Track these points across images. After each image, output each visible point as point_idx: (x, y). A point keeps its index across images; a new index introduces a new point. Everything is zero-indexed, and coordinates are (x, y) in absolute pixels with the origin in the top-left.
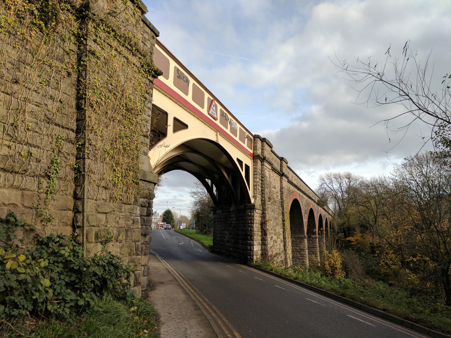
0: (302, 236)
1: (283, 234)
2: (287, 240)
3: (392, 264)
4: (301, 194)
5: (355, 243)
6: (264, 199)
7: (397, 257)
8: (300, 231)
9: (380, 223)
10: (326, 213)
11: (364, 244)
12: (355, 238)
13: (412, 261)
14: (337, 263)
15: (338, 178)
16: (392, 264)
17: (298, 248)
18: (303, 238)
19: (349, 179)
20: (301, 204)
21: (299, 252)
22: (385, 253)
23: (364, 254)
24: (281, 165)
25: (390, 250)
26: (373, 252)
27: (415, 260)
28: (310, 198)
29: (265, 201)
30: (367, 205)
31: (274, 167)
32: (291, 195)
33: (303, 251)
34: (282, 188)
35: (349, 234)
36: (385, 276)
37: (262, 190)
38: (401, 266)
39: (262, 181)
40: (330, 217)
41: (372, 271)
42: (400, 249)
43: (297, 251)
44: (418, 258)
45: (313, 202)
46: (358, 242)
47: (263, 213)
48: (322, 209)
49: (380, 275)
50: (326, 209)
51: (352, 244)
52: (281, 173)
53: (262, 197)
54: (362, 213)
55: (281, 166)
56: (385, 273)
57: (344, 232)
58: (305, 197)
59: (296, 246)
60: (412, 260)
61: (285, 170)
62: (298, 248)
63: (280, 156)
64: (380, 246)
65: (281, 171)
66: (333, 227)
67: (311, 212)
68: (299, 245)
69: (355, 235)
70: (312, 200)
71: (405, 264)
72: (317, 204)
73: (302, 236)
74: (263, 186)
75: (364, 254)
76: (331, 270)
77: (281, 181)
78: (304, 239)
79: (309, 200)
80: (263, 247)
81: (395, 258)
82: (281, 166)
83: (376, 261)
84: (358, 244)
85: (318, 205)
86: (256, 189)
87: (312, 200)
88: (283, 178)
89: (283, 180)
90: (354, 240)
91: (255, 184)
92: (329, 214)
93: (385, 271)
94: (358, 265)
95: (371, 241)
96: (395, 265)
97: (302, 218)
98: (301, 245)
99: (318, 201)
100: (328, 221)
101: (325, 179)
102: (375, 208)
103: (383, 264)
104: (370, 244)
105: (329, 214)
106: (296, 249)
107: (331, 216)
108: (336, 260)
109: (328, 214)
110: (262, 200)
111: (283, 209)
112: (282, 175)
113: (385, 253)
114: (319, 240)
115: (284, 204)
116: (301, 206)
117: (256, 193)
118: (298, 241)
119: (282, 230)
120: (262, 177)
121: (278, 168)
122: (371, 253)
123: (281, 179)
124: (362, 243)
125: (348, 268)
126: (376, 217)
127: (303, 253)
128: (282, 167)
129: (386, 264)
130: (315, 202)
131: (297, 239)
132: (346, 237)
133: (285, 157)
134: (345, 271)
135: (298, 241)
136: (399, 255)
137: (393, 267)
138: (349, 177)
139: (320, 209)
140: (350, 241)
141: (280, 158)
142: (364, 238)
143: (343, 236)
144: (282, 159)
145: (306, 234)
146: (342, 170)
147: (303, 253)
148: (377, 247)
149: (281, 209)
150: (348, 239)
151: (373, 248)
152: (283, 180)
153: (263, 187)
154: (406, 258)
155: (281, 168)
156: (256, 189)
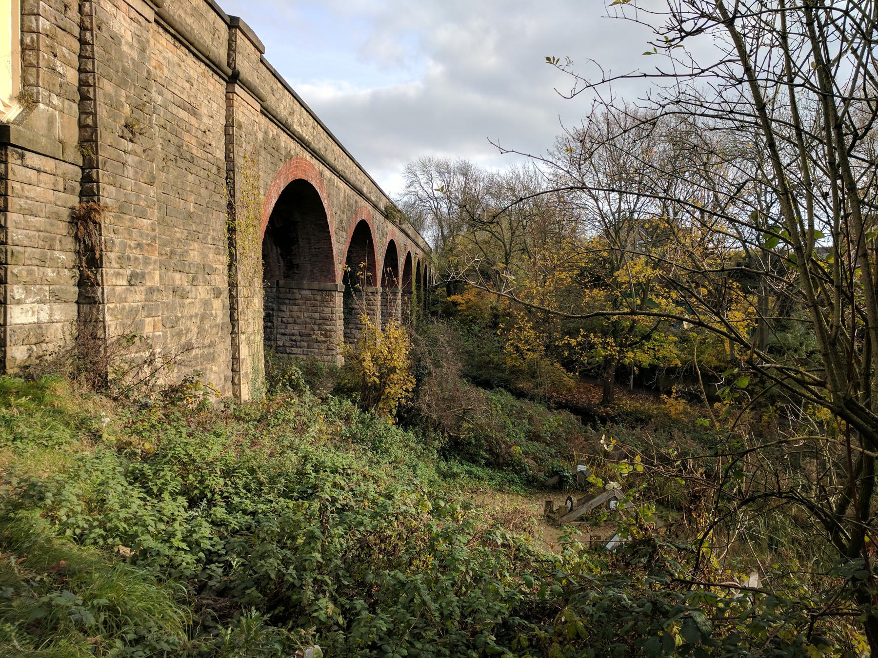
0: (329, 285)
1: (230, 270)
2: (243, 291)
3: (528, 350)
4: (328, 173)
5: (463, 307)
6: (89, 121)
7: (538, 337)
8: (325, 274)
9: (515, 267)
10: (409, 242)
11: (481, 310)
12: (465, 297)
13: (568, 345)
14: (395, 356)
15: (444, 173)
16: (528, 350)
17: (317, 315)
18: (330, 292)
19: (465, 175)
20: (326, 203)
21: (319, 324)
22: (517, 328)
23: (477, 328)
24: (230, 45)
25: (528, 322)
26: (495, 326)
27: (573, 342)
28: (361, 193)
29: (94, 128)
30: (493, 230)
31: (166, 15)
32: (282, 165)
33: (328, 322)
34: (230, 124)
35: (455, 288)
36: (512, 373)
37: (83, 83)
38: (543, 353)
39: (82, 42)
40: (419, 251)
41: (489, 363)
42: (546, 320)
43: (315, 324)
44: (580, 339)
45: (370, 208)
46: (470, 304)
47: (87, 179)
48: (397, 232)
49: (503, 371)
50: (410, 233)
51: (459, 308)
52: (230, 72)
53: (83, 112)
54: (483, 246)
55: (231, 48)
56: (514, 366)
57: (448, 287)
58: (342, 185)
59: (312, 311)
60: (569, 343)
61: (245, 66)
62: (317, 315)
63: (229, 10)
64: (509, 314)
65: (229, 65)
66: (425, 274)
67: (392, 245)
68: (319, 309)
69: (466, 292)
70: (368, 199)
71: (550, 349)
72: (382, 213)
73: (329, 285)
74: (89, 67)
75: (477, 328)
76: (377, 374)
77: (228, 98)
78: (333, 293)
79: (357, 197)
80: (85, 308)
81: (536, 339)
82: (231, 48)
83: (499, 342)
84: (469, 308)
85: (386, 217)
86: (31, 65)
87: (368, 199)
88: (237, 89)
89: (235, 97)
90: (462, 302)
91: (28, 40)
92: (418, 245)
93: (514, 363)
94: (448, 360)
95: (494, 304)
96: (533, 351)
97: (329, 238)
98: (326, 309)
99: (386, 208)
100: (413, 259)
101: (418, 173)
102: (507, 235)
103: (511, 349)
104: (492, 308)
105: (418, 245)
106: (311, 318)
107: (422, 250)
108: (395, 349)
109: (413, 244)
110: (82, 126)
111: (232, 195)
112: (233, 78)
113: (517, 328)
114: (383, 298)
115: (237, 178)
116: (325, 206)
117: (32, 80)
118: (319, 298)
119: (225, 259)
120: (83, 28)
121: (220, 53)
122: (490, 327)
123: (229, 92)
124: (478, 306)
125: (424, 368)
126: (507, 256)
127: (328, 328)
128: (235, 51)
129: (517, 349)
130: (375, 207)
131: (315, 292)
132: (449, 294)
133: (247, 19)
134: (416, 377)
135: (319, 298)
136: (544, 332)
137: (530, 356)
138: (465, 171)
139: (390, 227)
140: (455, 304)
141: (228, 21)
142: (482, 298)
143: (445, 293)
144: (233, 23)
145: (339, 281)
146: (453, 158)
147: (328, 328)
148: (504, 316)
149: (225, 192)
150: (453, 298)
151: (496, 316)
152: (235, 97)
153: (87, 72)
154: (557, 340)
155: (229, 55)
156: (31, 65)
